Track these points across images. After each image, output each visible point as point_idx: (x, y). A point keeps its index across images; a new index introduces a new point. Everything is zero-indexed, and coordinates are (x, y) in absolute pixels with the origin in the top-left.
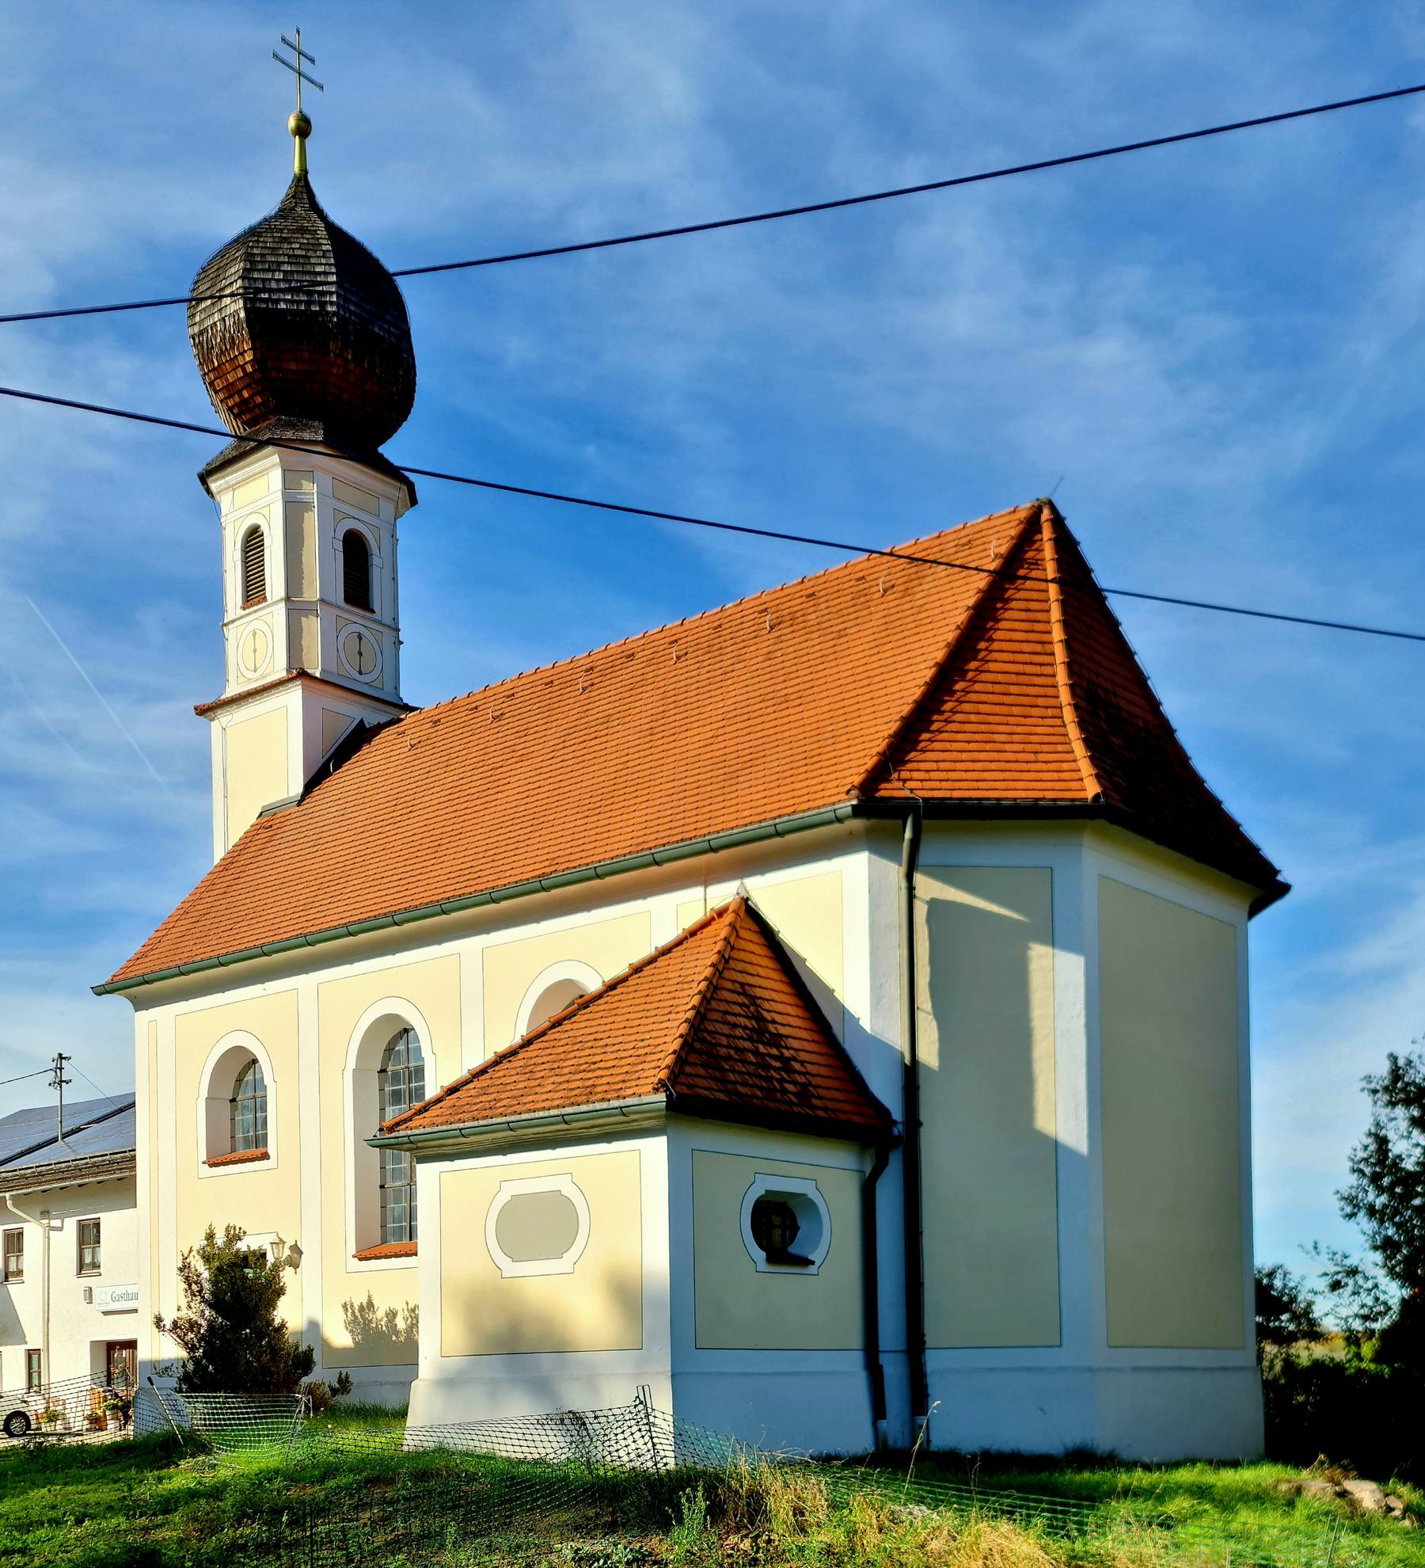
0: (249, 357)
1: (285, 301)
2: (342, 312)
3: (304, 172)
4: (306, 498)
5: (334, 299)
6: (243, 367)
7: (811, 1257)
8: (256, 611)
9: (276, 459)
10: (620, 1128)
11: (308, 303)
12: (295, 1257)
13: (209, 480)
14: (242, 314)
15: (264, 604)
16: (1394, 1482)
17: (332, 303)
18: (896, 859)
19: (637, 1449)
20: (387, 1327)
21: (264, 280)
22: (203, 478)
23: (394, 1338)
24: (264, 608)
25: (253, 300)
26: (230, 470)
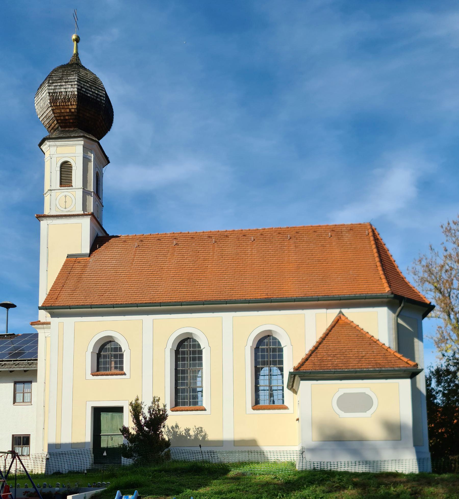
0: (75, 107)
1: (90, 94)
3: (77, 54)
4: (89, 158)
5: (104, 99)
6: (70, 109)
8: (67, 189)
9: (82, 143)
10: (378, 376)
14: (76, 93)
15: (71, 188)
18: (394, 312)
19: (345, 465)
20: (185, 434)
23: (188, 438)
24: (71, 189)
25: (81, 90)
26: (59, 140)
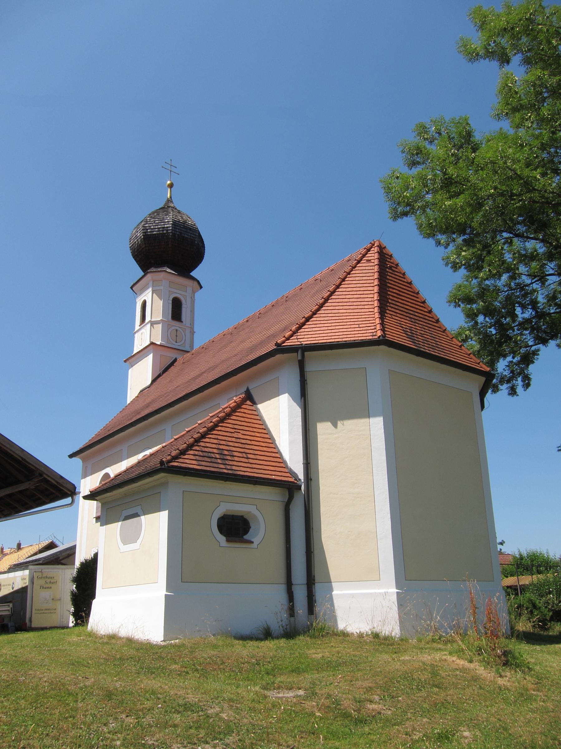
2: (173, 232)
7: (252, 540)
11: (163, 231)
12: (518, 395)
13: (133, 289)
16: (331, 622)
17: (170, 230)
21: (149, 226)
22: (132, 288)
